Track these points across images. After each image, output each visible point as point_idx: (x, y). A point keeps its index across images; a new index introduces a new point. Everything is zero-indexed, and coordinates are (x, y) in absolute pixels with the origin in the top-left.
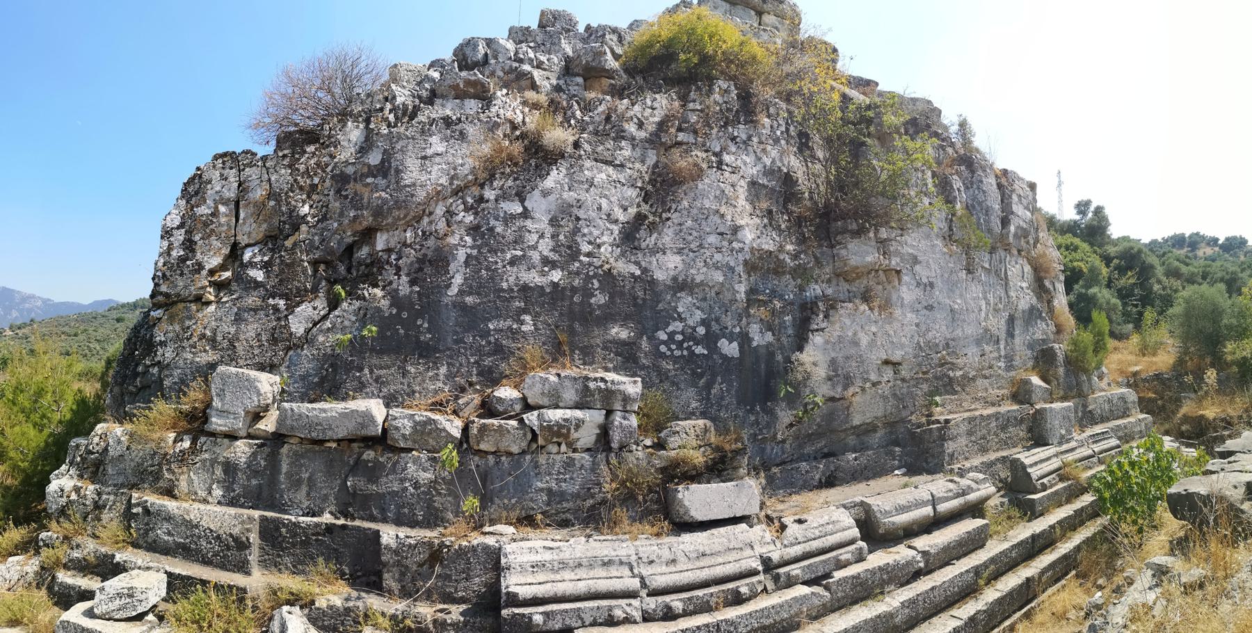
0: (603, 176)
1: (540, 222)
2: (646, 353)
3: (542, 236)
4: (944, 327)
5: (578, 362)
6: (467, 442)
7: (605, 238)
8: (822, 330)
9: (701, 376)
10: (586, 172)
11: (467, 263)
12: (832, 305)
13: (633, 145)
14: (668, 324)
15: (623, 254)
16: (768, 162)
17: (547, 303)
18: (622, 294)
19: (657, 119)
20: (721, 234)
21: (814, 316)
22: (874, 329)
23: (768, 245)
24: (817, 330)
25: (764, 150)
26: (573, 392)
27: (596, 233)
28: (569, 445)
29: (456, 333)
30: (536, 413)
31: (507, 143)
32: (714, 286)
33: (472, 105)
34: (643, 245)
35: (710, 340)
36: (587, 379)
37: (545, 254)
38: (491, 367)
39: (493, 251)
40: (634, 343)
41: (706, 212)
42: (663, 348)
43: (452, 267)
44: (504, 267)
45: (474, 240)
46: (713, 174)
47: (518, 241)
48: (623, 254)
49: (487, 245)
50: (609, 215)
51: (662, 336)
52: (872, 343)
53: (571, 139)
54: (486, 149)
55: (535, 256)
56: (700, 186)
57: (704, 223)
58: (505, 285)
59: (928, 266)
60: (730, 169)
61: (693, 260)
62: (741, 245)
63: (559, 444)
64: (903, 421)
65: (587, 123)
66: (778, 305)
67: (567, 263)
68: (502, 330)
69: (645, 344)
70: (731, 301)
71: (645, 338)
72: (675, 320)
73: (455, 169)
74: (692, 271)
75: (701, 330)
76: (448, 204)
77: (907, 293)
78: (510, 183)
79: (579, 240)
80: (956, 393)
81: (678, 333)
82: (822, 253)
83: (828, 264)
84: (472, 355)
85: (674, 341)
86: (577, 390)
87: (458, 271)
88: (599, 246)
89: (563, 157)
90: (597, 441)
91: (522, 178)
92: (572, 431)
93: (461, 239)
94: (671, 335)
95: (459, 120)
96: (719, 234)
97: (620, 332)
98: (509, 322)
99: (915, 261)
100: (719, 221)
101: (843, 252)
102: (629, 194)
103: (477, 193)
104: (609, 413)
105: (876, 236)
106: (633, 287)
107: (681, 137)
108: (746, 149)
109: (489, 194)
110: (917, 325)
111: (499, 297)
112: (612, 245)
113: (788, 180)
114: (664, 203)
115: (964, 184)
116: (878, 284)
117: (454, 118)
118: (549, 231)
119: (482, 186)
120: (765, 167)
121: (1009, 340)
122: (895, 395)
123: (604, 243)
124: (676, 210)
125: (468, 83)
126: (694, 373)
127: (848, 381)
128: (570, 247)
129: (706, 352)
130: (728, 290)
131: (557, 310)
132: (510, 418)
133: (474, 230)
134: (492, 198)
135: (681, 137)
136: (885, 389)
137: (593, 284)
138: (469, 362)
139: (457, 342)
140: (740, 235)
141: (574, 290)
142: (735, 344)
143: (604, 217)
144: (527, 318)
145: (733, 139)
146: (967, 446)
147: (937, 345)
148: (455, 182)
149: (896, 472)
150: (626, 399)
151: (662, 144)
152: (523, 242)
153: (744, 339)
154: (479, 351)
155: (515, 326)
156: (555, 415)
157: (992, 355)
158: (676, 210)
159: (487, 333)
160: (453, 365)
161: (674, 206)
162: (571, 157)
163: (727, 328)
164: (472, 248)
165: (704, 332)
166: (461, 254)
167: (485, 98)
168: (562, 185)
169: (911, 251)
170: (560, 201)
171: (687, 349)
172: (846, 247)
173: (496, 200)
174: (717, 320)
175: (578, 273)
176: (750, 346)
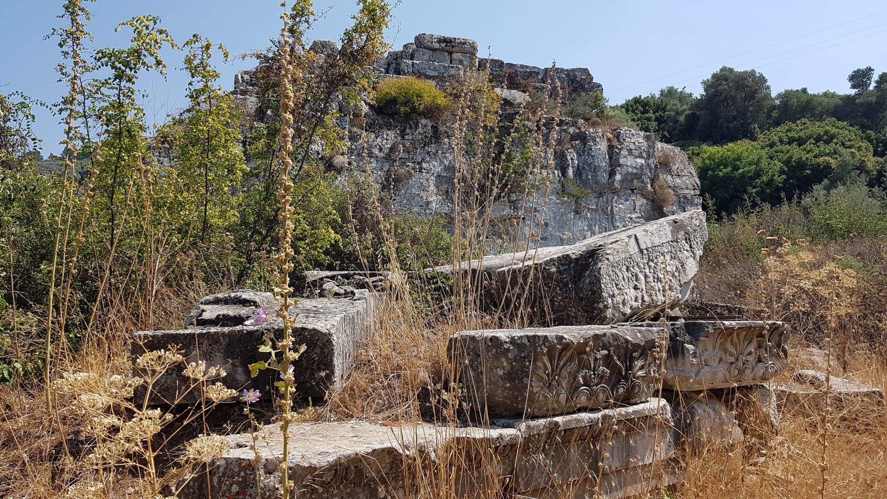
16: (447, 163)
19: (389, 146)
20: (421, 206)
25: (445, 157)
46: (417, 175)
56: (410, 182)
60: (426, 171)
62: (431, 211)
105: (508, 198)
115: (577, 153)
140: (430, 206)
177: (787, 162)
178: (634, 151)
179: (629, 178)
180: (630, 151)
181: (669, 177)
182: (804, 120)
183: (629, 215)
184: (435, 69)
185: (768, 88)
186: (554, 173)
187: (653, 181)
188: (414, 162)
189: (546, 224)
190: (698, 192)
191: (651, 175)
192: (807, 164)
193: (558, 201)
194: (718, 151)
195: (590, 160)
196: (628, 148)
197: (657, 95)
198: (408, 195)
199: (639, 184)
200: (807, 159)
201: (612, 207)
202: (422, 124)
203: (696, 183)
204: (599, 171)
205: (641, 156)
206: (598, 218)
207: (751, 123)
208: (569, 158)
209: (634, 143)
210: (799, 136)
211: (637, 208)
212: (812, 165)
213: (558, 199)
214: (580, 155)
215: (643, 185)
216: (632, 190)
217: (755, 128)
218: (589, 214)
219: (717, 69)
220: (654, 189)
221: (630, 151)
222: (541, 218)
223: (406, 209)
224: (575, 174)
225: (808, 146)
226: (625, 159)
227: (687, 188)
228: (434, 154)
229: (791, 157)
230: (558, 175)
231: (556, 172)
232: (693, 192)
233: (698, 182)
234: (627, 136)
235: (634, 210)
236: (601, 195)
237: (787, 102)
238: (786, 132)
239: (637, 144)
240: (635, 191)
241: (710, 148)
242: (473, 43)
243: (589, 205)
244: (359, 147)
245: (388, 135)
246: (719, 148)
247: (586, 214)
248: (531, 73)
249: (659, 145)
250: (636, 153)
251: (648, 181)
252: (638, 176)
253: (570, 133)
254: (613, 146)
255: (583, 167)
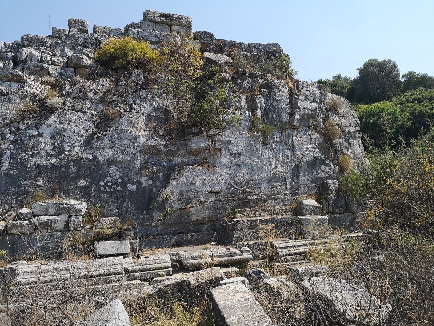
0: (76, 117)
1: (46, 138)
2: (94, 191)
3: (47, 144)
4: (246, 175)
5: (63, 196)
6: (7, 231)
7: (77, 144)
8: (177, 179)
9: (119, 199)
10: (68, 116)
11: (11, 157)
12: (182, 166)
13: (92, 102)
14: (105, 178)
15: (85, 150)
17: (49, 172)
18: (84, 167)
19: (104, 90)
20: (130, 140)
21: (173, 173)
22: (204, 177)
23: (152, 143)
24: (174, 179)
25: (155, 100)
26: (54, 209)
27: (72, 141)
28: (52, 229)
29: (6, 186)
30: (37, 218)
31: (31, 103)
32: (125, 162)
33: (16, 86)
34: (94, 146)
35: (124, 184)
36: (60, 204)
37: (48, 151)
38: (22, 200)
39: (23, 151)
40: (89, 187)
41: (123, 131)
42: (102, 189)
43: (4, 158)
44: (29, 157)
45: (14, 146)
47: (36, 146)
48: (85, 150)
49: (20, 148)
50: (78, 134)
51: (102, 183)
52: (203, 184)
53: (62, 101)
54: (21, 106)
55: (44, 153)
56: (121, 120)
57: (122, 135)
58: (29, 166)
59: (237, 145)
61: (117, 152)
62: (138, 144)
63: (48, 229)
64: (219, 220)
65: (71, 93)
66: (155, 169)
67: (59, 155)
68: (28, 184)
69: (94, 187)
70: (133, 168)
71: (94, 185)
72: (108, 177)
73: (6, 115)
74: (116, 156)
75: (120, 181)
76: (2, 130)
77: (224, 159)
78: (32, 121)
79: (64, 145)
80: (252, 207)
81: (110, 182)
82: (180, 144)
83: (183, 149)
84: (13, 195)
85: (107, 186)
86: (55, 208)
87: (7, 160)
88: (74, 147)
89: (57, 109)
90: (64, 228)
91: (37, 119)
92: (53, 224)
93: (8, 146)
94: (106, 183)
95: (8, 93)
96: (129, 140)
97: (82, 183)
98: (31, 181)
99: (230, 143)
100: (129, 135)
101: (190, 143)
102: (89, 124)
103: (16, 126)
104: (70, 217)
105: (207, 133)
106: (89, 164)
107: (114, 98)
108: (145, 101)
109: (22, 126)
110: (230, 174)
111: (26, 170)
112: (80, 146)
113: (166, 111)
114: (104, 128)
115: (265, 98)
116: (211, 155)
117: (5, 92)
118: (50, 142)
119: (19, 123)
120: (154, 108)
121: (294, 179)
122: (215, 208)
123: (76, 146)
124: (110, 131)
125: (13, 75)
126: (116, 198)
127: (189, 201)
128: (60, 148)
129: (122, 189)
130: (132, 163)
131: (53, 175)
132: (26, 220)
133: (14, 142)
134: (23, 128)
135: (114, 98)
136: (209, 204)
137: (70, 163)
138: (12, 198)
139: (6, 190)
140: (138, 140)
141: (61, 166)
142: (135, 186)
143: (76, 135)
144: (40, 179)
145: (140, 97)
146: (249, 234)
147: (241, 183)
148: (6, 121)
149: (213, 243)
150: (77, 211)
151: (105, 102)
152: (38, 147)
153: (139, 183)
154: (17, 194)
155: (33, 183)
156: (45, 218)
157: (279, 188)
158: (110, 131)
159: (20, 186)
160: (4, 200)
161: (109, 129)
162: (60, 109)
163: (131, 179)
164: (13, 150)
165: (121, 181)
166: (8, 153)
167: (22, 82)
168: (56, 122)
169: (227, 139)
170: (55, 129)
171: (113, 188)
172: (190, 141)
173: (25, 129)
174: (127, 176)
175: (63, 159)
176: (141, 186)
177: (413, 113)
178: (309, 97)
179: (306, 117)
180: (306, 97)
181: (337, 118)
182: (420, 89)
183: (306, 146)
184: (156, 36)
185: (399, 70)
186: (245, 113)
187: (324, 120)
188: (126, 104)
189: (239, 154)
190: (358, 129)
191: (323, 116)
192: (425, 114)
193: (249, 135)
194: (369, 108)
195: (275, 104)
196: (305, 95)
197: (331, 79)
198: (118, 131)
199: (314, 122)
200: (425, 111)
201: (293, 140)
202: (135, 73)
203: (357, 122)
204: (281, 112)
205: (315, 101)
206: (281, 148)
207: (388, 91)
208: (258, 102)
209: (309, 91)
210: (419, 98)
211: (313, 140)
212: (428, 114)
213: (249, 134)
214: (267, 100)
215: (317, 123)
216: (309, 127)
217: (390, 94)
218: (274, 145)
219: (366, 60)
220: (326, 126)
221: (306, 97)
222: (234, 148)
223: (116, 142)
224: (263, 115)
225: (426, 102)
226: (303, 103)
227: (350, 126)
228: (145, 98)
229: (415, 110)
230: (249, 115)
231: (247, 112)
232: (355, 128)
233: (359, 122)
234: (304, 85)
235: (310, 142)
236: (283, 130)
237: (410, 78)
238: (410, 96)
239: (311, 92)
240: (311, 128)
241: (363, 106)
242: (188, 18)
243: (274, 138)
244: (75, 91)
245: (104, 81)
246: (369, 106)
247: (272, 145)
248: (238, 45)
249: (329, 95)
250: (311, 98)
251: (321, 120)
252: (313, 116)
253: (259, 84)
254: (293, 93)
255: (270, 110)
